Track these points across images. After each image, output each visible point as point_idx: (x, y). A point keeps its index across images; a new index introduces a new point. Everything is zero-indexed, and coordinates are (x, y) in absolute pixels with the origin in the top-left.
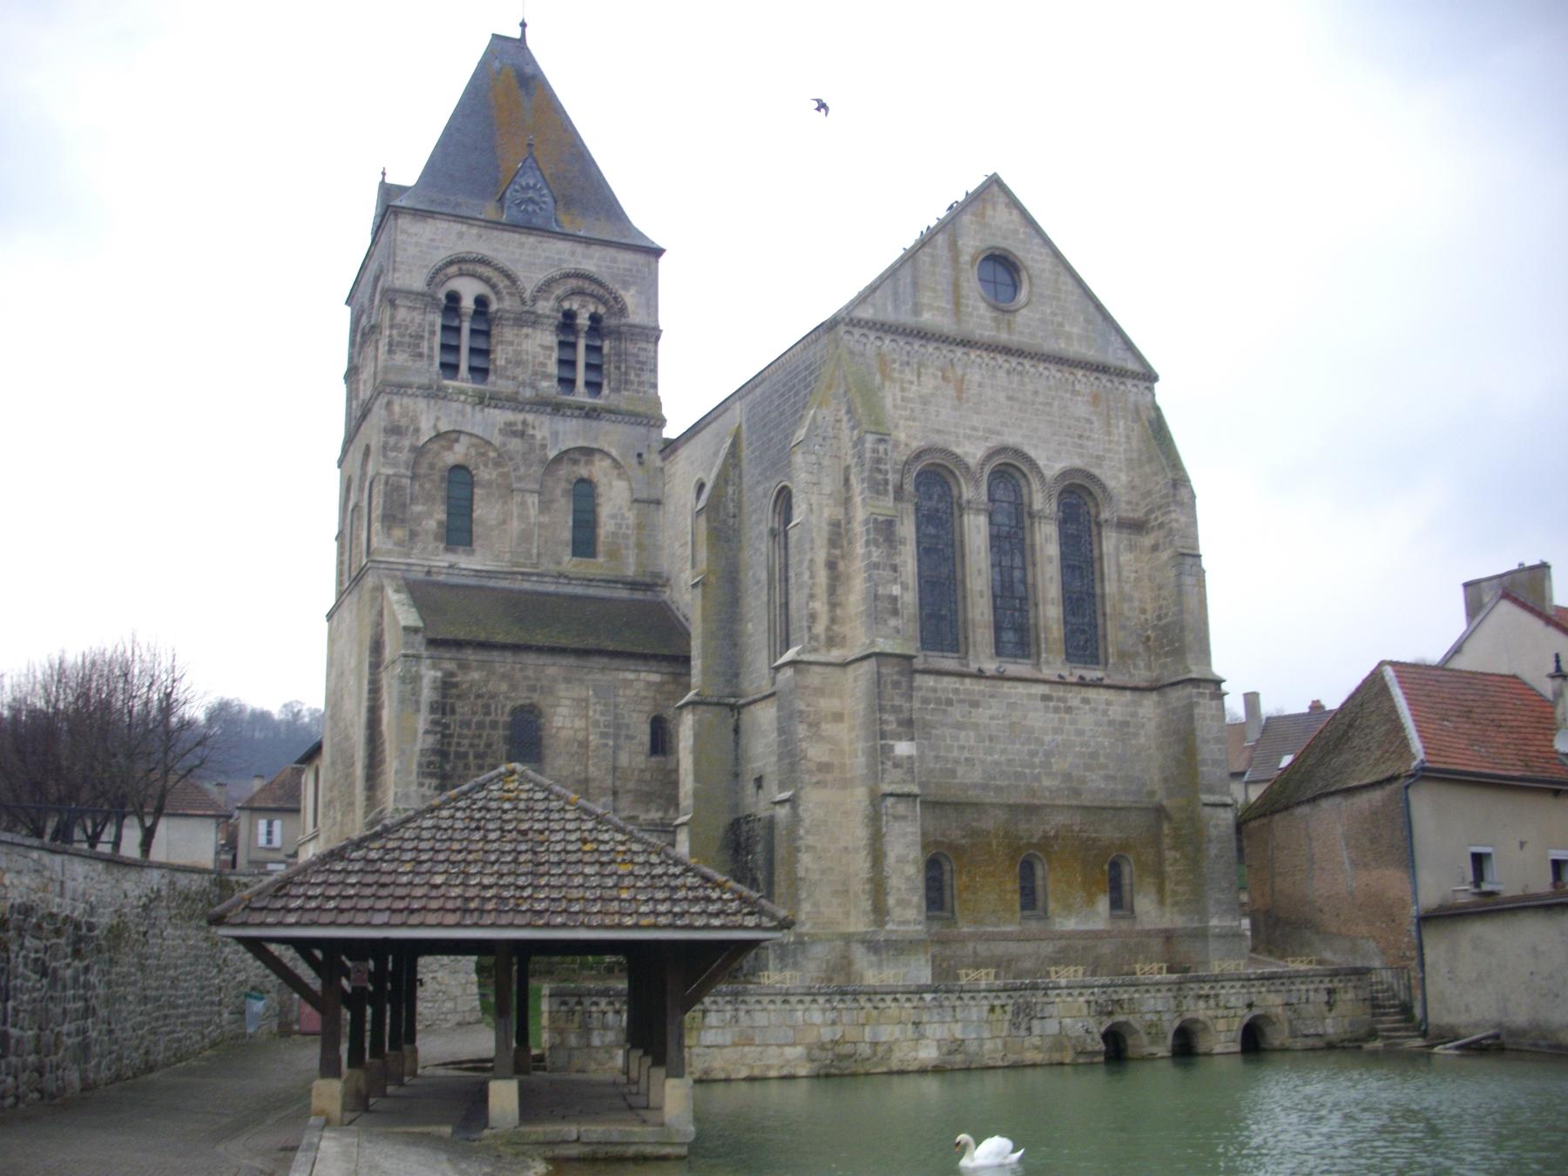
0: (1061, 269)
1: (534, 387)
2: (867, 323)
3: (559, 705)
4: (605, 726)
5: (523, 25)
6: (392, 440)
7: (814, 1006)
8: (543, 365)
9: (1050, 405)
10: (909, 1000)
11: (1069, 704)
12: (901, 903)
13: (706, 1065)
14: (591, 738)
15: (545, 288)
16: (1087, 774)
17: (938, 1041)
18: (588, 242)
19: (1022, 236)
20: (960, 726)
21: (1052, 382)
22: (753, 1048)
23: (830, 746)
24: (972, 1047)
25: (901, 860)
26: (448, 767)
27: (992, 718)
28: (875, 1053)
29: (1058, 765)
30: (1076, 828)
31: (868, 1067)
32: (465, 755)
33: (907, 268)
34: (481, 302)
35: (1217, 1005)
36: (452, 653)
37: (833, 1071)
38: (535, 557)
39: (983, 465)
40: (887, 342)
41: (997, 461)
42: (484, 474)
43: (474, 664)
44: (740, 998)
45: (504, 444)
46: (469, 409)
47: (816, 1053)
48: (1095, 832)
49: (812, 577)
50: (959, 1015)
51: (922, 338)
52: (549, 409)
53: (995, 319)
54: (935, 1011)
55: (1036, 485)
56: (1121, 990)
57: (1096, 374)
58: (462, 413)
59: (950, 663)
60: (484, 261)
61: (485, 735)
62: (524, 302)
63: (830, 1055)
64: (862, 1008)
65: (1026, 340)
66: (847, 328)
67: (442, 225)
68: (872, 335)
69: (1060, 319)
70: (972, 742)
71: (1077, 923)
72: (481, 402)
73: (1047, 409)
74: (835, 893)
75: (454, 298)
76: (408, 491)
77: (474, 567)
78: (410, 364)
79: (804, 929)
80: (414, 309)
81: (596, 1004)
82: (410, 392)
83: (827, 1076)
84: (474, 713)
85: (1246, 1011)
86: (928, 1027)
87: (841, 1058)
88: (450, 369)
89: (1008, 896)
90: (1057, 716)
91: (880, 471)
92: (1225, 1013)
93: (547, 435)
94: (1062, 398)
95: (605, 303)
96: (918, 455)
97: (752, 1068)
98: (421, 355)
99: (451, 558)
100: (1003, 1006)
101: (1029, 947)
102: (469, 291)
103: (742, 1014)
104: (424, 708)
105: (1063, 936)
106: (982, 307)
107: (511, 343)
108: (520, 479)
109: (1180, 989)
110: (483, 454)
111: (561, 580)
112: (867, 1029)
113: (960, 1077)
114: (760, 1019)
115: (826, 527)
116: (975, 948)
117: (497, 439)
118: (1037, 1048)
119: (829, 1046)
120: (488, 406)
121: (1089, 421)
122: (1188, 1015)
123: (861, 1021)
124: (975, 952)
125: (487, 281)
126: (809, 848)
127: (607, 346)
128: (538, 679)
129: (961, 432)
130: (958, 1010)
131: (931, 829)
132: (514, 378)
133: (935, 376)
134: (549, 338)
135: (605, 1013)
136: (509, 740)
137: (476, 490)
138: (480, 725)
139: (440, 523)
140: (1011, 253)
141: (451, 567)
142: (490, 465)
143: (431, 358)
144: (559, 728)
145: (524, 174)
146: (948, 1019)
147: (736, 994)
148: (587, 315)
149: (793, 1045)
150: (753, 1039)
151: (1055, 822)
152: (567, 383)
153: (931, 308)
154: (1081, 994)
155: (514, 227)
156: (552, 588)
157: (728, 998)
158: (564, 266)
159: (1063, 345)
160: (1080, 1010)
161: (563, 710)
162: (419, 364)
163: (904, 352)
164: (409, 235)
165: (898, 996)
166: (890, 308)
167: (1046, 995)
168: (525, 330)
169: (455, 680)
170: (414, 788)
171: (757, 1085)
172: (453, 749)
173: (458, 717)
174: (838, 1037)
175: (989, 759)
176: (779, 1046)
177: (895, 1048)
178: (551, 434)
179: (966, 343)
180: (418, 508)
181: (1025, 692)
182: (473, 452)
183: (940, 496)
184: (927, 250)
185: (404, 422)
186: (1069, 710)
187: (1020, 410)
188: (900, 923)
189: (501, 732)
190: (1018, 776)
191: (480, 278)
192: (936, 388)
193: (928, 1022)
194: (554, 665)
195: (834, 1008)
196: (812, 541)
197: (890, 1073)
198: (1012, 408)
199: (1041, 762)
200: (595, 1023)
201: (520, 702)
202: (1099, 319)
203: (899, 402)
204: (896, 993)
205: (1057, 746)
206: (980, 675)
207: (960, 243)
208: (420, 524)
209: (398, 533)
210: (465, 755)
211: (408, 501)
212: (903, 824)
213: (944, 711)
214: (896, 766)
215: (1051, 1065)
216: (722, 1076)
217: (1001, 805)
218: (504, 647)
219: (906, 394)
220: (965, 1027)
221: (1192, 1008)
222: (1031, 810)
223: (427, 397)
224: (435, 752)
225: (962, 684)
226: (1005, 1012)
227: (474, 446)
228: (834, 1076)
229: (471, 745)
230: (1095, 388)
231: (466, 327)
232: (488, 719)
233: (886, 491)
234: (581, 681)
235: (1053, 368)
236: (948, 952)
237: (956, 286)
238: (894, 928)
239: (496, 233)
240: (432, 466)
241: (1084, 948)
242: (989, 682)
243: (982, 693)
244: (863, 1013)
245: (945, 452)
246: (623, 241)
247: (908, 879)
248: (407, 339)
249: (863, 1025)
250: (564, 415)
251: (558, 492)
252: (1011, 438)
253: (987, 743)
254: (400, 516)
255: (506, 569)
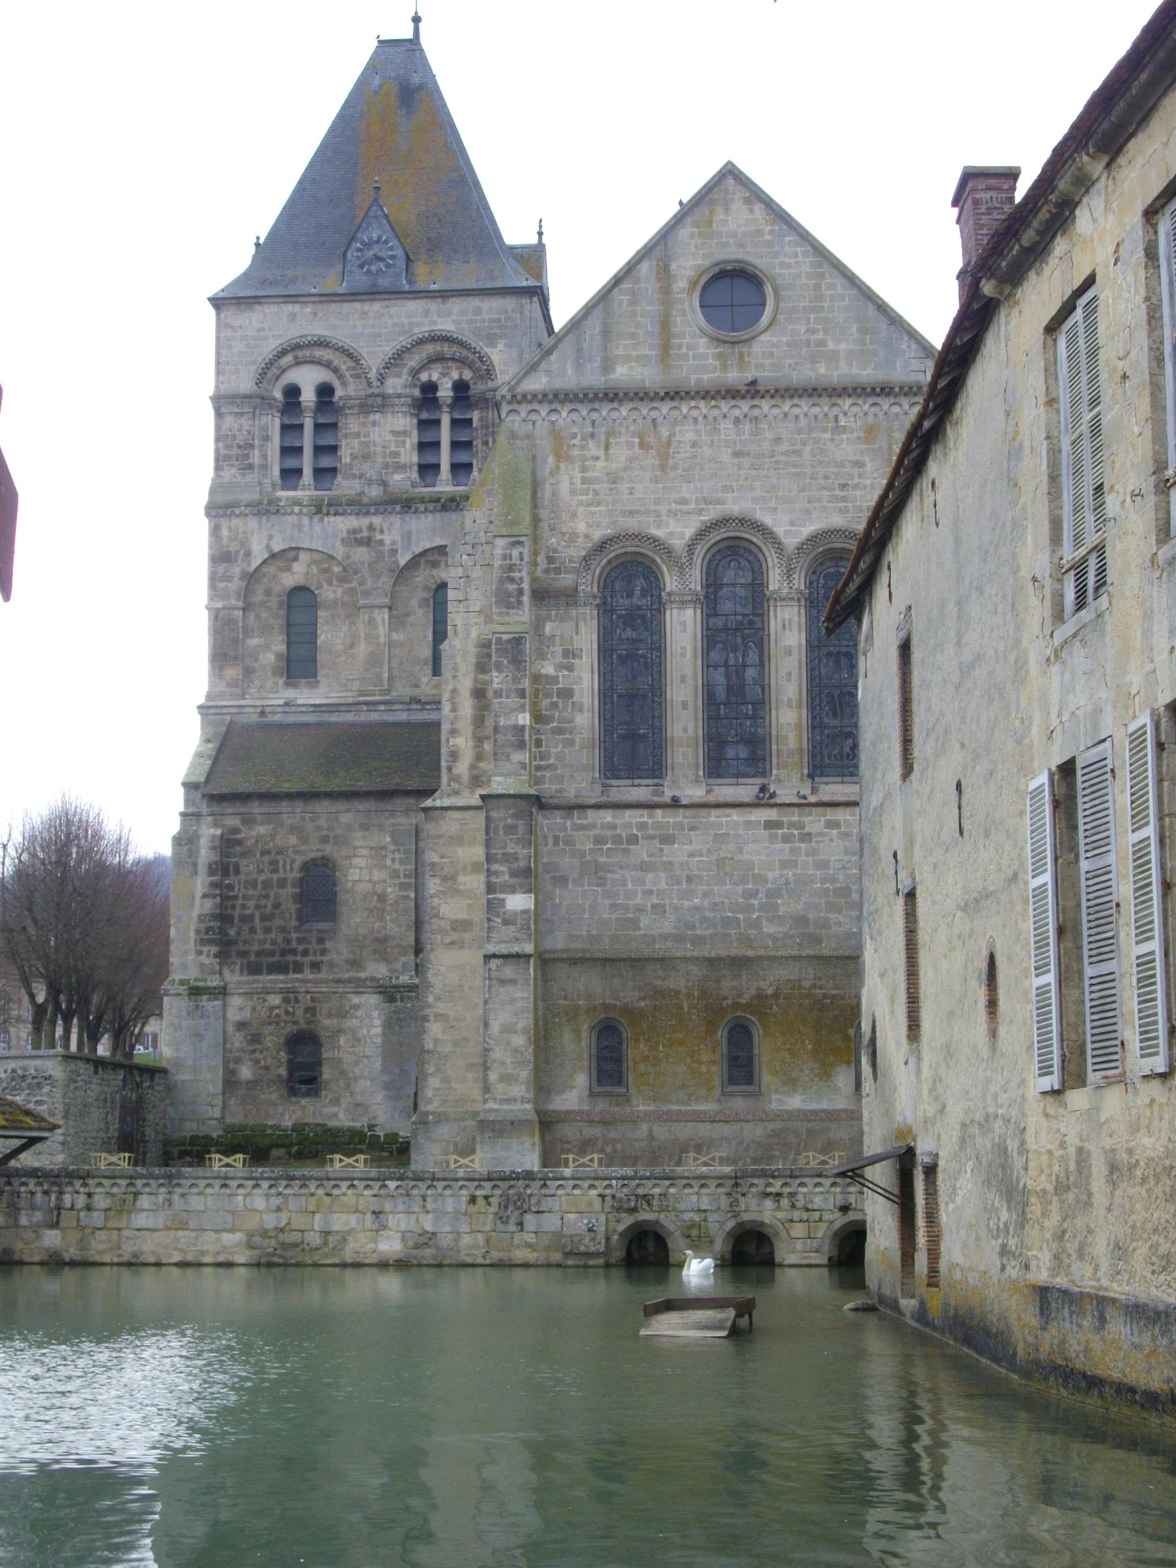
0: (826, 268)
1: (384, 484)
2: (535, 396)
3: (354, 856)
4: (406, 876)
5: (416, 20)
6: (221, 569)
7: (257, 1191)
8: (396, 454)
9: (798, 453)
10: (367, 1187)
11: (807, 830)
12: (505, 1078)
13: (136, 1248)
14: (389, 890)
15: (399, 356)
16: (831, 916)
17: (403, 1232)
18: (444, 295)
19: (768, 237)
20: (645, 867)
21: (803, 421)
22: (187, 1233)
23: (468, 901)
24: (446, 1241)
25: (508, 1029)
26: (232, 932)
27: (691, 855)
28: (326, 1243)
29: (785, 906)
30: (807, 984)
31: (316, 1257)
32: (252, 917)
33: (597, 313)
34: (325, 391)
35: (793, 1206)
36: (239, 808)
37: (276, 1260)
38: (385, 682)
39: (691, 547)
40: (564, 414)
41: (722, 533)
42: (328, 593)
43: (260, 818)
44: (175, 1181)
45: (348, 557)
46: (306, 520)
47: (257, 1240)
48: (836, 987)
49: (454, 710)
50: (430, 1205)
51: (612, 401)
52: (398, 508)
53: (719, 356)
54: (401, 1200)
55: (772, 558)
56: (650, 1183)
57: (871, 400)
58: (299, 527)
59: (641, 792)
60: (322, 343)
61: (272, 895)
62: (370, 384)
63: (273, 1242)
64: (313, 1195)
65: (766, 374)
66: (510, 407)
67: (271, 309)
68: (544, 410)
69: (821, 336)
70: (663, 885)
71: (803, 1101)
72: (319, 512)
73: (794, 458)
74: (470, 1066)
75: (293, 392)
76: (241, 624)
77: (313, 702)
78: (239, 478)
79: (430, 1108)
80: (242, 414)
81: (25, 1184)
82: (237, 511)
83: (269, 1265)
84: (260, 871)
85: (838, 1214)
86: (390, 1217)
87: (284, 1246)
88: (290, 475)
89: (704, 1068)
90: (787, 846)
91: (512, 580)
92: (805, 1216)
93: (398, 538)
94: (817, 441)
95: (470, 366)
96: (602, 546)
97: (185, 1252)
98: (251, 467)
99: (290, 694)
100: (486, 1197)
101: (727, 1130)
102: (308, 380)
103: (176, 1197)
104: (202, 870)
105: (778, 1116)
106: (702, 345)
107: (357, 435)
108: (367, 594)
109: (736, 1185)
110: (326, 571)
111: (414, 706)
112: (318, 1217)
113: (428, 1274)
114: (196, 1203)
115: (472, 649)
116: (650, 1130)
117: (339, 551)
118: (529, 1246)
119: (273, 1234)
120: (328, 514)
121: (859, 464)
122: (746, 1217)
123: (310, 1208)
124: (651, 1136)
125: (328, 365)
126: (440, 1017)
127: (476, 416)
128: (330, 829)
129: (663, 509)
130: (429, 1200)
131: (598, 990)
132: (361, 476)
133: (630, 445)
134: (402, 421)
135: (33, 1193)
136: (300, 898)
137: (319, 613)
138: (267, 884)
139: (279, 656)
140: (749, 264)
141: (286, 704)
142: (335, 583)
143: (264, 467)
144: (355, 882)
145: (369, 224)
146: (416, 1209)
147: (170, 1177)
148: (450, 385)
149: (232, 1230)
150: (187, 1223)
151: (770, 979)
152: (428, 470)
153: (627, 359)
154: (592, 1187)
155: (353, 296)
156: (403, 717)
157: (162, 1181)
158: (416, 330)
159: (822, 371)
160: (590, 1204)
161: (360, 862)
162: (248, 478)
163: (588, 422)
164: (233, 328)
165: (355, 1182)
166: (570, 371)
167: (545, 1185)
168: (372, 417)
169: (238, 836)
170: (191, 957)
171: (190, 1272)
172: (237, 913)
173: (242, 877)
174: (282, 1225)
175: (686, 903)
176: (216, 1231)
177: (350, 1238)
178: (402, 536)
179: (674, 395)
180: (254, 642)
181: (741, 819)
182: (315, 569)
183: (642, 590)
184: (625, 286)
185: (233, 547)
186: (807, 837)
187: (753, 467)
188: (502, 1101)
189: (290, 890)
190: (727, 922)
191: (319, 362)
192: (631, 459)
193: (391, 1212)
194: (348, 811)
195: (280, 1194)
196: (456, 669)
197: (344, 1265)
198: (739, 467)
199: (761, 905)
200: (23, 1204)
201: (312, 855)
202: (883, 325)
203: (578, 485)
204: (354, 1179)
205: (787, 883)
206: (675, 803)
207: (674, 266)
208: (256, 660)
209: (231, 672)
210: (252, 917)
211: (241, 636)
212: (511, 989)
213: (626, 851)
214: (506, 922)
215: (548, 1266)
216: (152, 1260)
217: (697, 959)
218: (290, 796)
219: (589, 474)
220: (436, 1218)
221: (753, 1207)
222: (738, 963)
223: (259, 514)
224: (214, 917)
225: (651, 816)
226: (489, 1204)
227: (315, 562)
228: (278, 1265)
229: (257, 907)
230: (870, 418)
231: (308, 424)
232: (275, 877)
233: (520, 602)
234: (381, 827)
235: (804, 404)
236: (613, 1135)
237: (665, 326)
238: (495, 1106)
239: (333, 306)
240: (268, 592)
241: (810, 1132)
242: (688, 812)
243: (681, 826)
244: (313, 1200)
245: (638, 536)
246: (489, 285)
247: (516, 1051)
248: (235, 451)
249: (313, 1213)
250: (416, 511)
251: (415, 603)
252: (734, 506)
253: (684, 886)
254: (232, 653)
255: (350, 700)
